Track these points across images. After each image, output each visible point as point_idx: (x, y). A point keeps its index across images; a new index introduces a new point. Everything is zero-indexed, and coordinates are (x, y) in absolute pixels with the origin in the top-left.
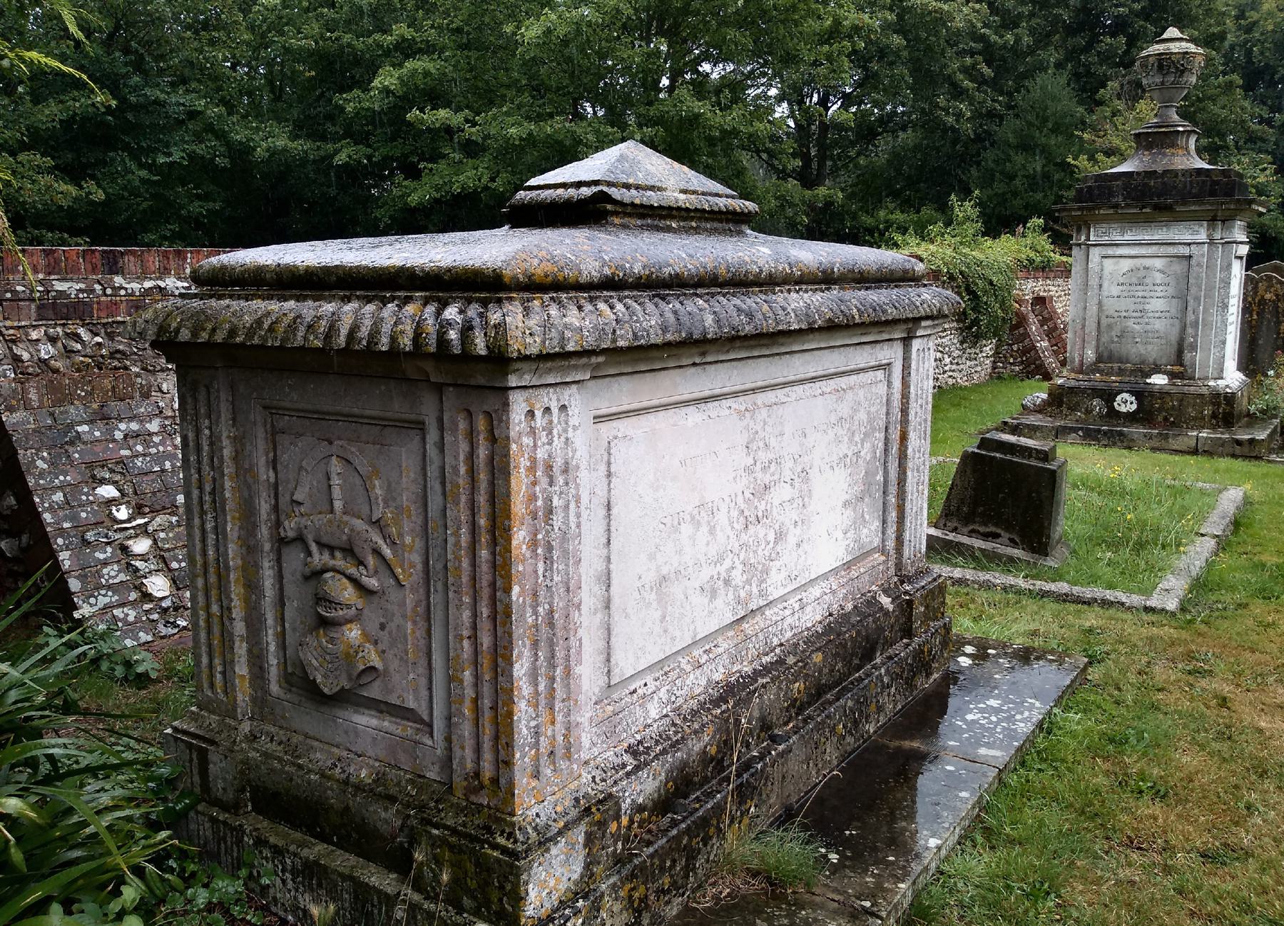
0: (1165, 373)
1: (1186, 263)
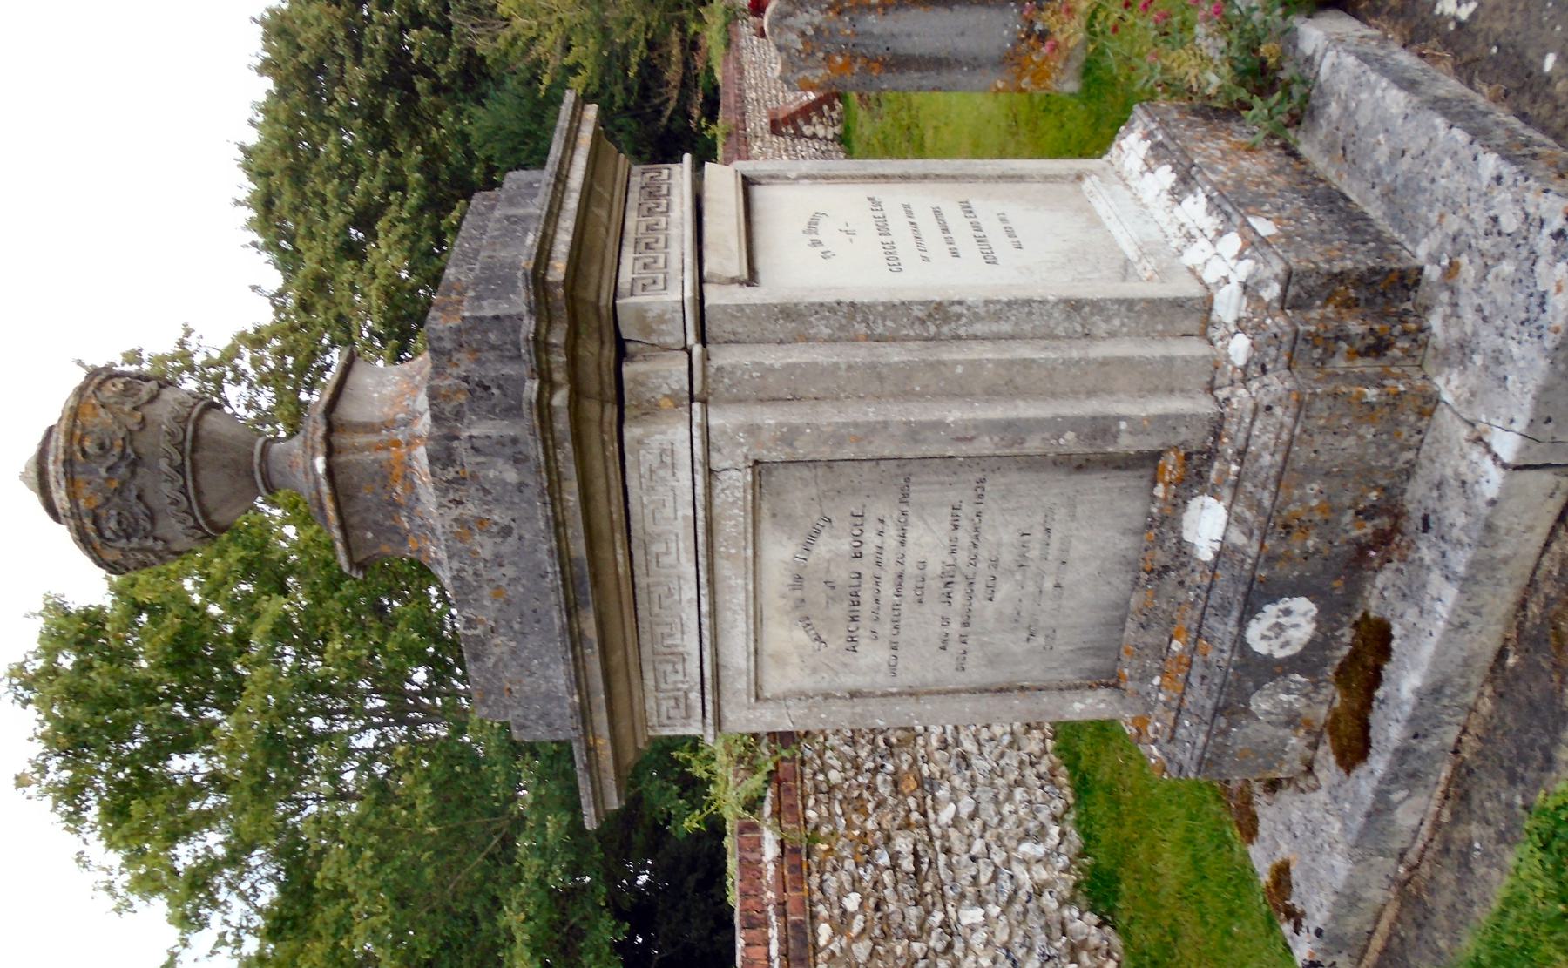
0: (1178, 504)
1: (779, 475)
